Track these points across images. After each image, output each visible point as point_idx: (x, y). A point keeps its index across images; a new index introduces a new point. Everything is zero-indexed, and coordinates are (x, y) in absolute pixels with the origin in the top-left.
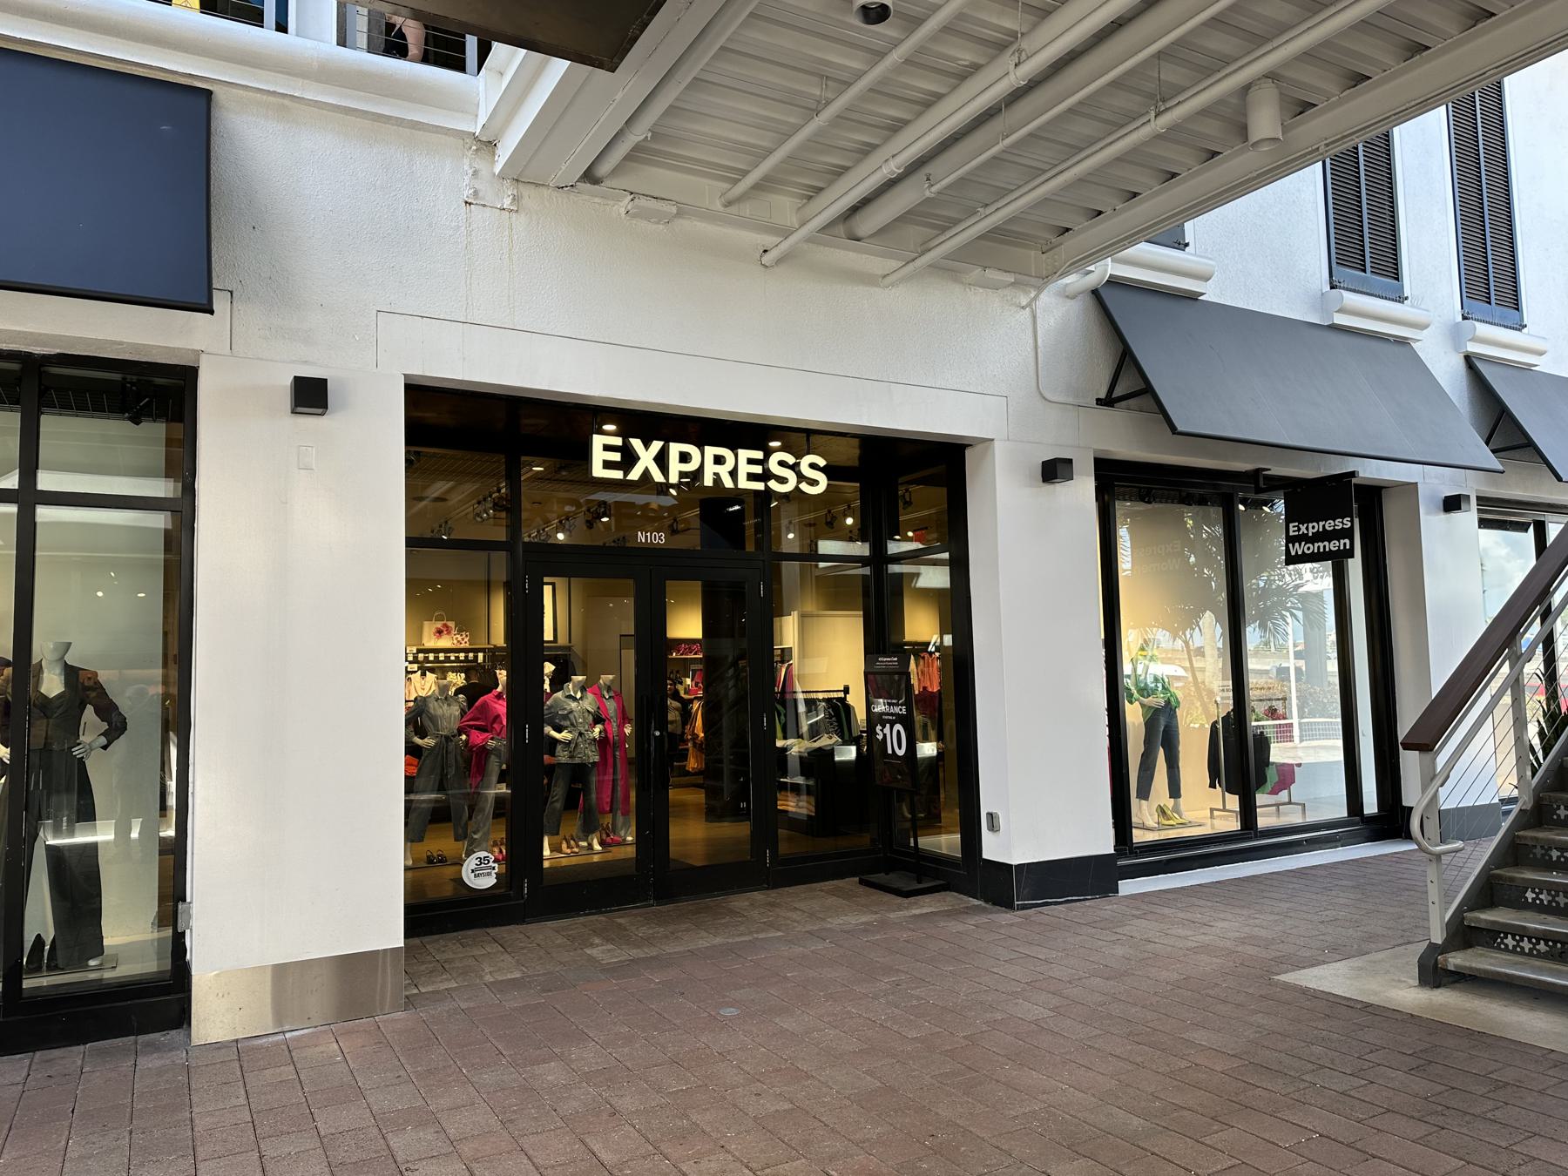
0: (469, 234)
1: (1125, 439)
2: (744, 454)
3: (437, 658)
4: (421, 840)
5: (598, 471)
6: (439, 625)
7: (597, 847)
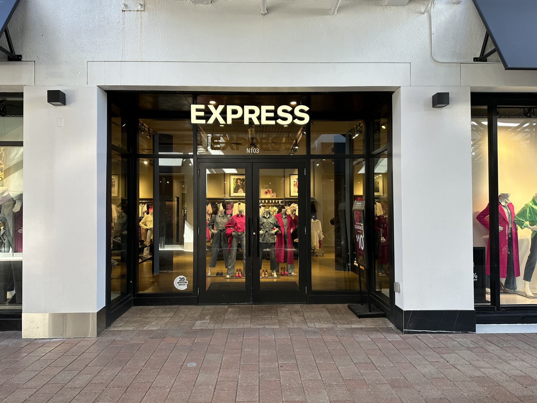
0: (124, 24)
1: (494, 80)
2: (264, 108)
3: (265, 202)
4: (214, 266)
5: (194, 120)
6: (266, 190)
7: (275, 276)
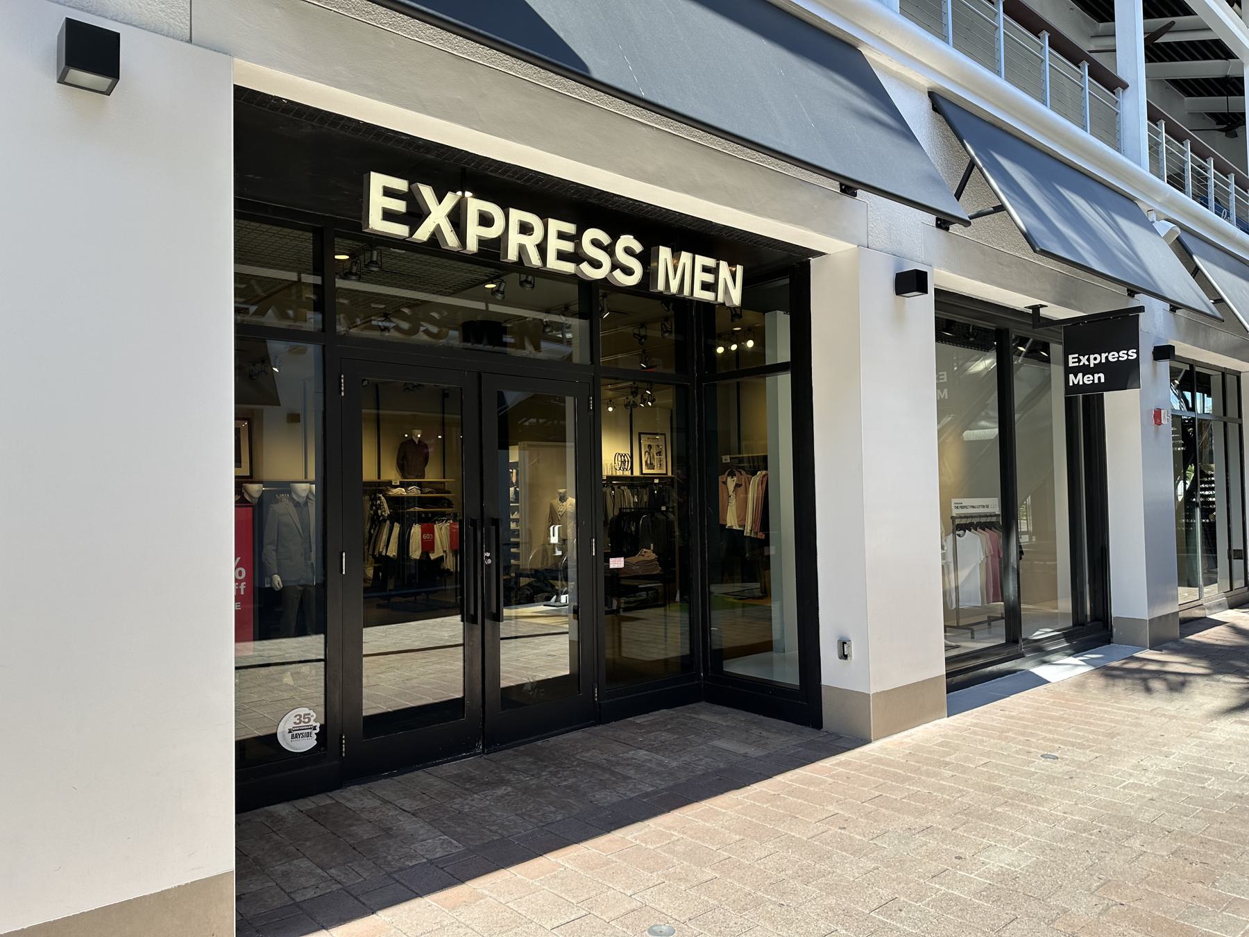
2: (555, 225)
